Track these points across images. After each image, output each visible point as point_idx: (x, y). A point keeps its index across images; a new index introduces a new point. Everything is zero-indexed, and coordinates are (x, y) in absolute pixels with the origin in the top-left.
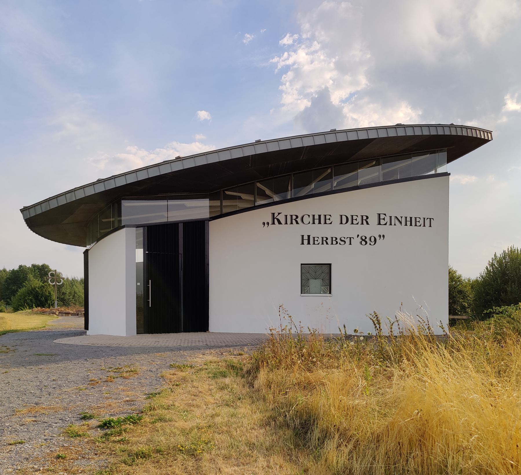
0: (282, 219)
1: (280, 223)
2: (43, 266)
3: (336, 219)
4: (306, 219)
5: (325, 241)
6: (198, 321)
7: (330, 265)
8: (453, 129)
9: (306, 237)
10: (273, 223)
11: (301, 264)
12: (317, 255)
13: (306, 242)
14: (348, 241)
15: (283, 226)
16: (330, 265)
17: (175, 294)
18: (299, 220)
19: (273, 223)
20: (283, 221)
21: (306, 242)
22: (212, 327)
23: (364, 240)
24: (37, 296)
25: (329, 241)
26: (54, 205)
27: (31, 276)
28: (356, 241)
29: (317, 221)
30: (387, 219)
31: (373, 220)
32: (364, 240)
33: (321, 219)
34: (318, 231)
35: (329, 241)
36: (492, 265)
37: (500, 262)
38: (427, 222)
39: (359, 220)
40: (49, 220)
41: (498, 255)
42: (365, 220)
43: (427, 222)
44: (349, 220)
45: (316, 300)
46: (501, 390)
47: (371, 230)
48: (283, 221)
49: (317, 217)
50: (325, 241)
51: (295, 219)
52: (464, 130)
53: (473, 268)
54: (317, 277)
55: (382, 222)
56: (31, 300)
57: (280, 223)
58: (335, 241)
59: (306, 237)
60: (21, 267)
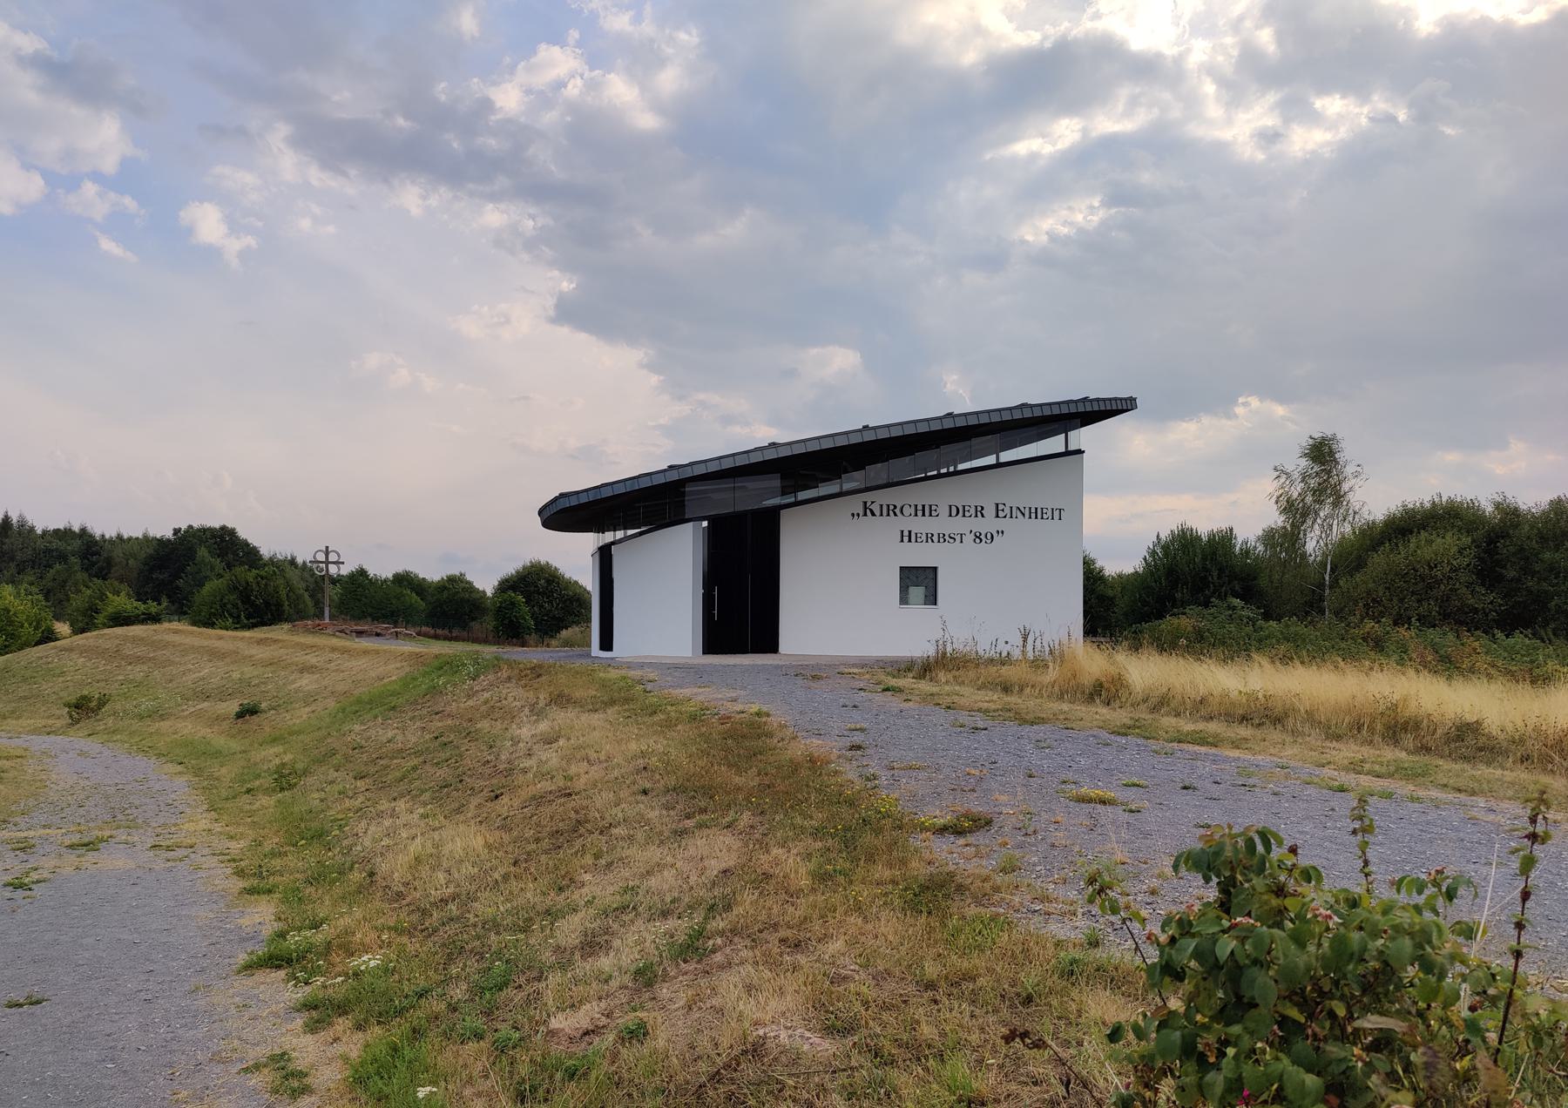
2: (223, 528)
4: (907, 510)
6: (769, 643)
7: (935, 569)
12: (919, 556)
14: (958, 538)
15: (878, 518)
16: (935, 569)
17: (741, 610)
22: (783, 648)
23: (978, 537)
24: (248, 598)
27: (202, 552)
28: (969, 538)
30: (1007, 511)
31: (990, 511)
32: (978, 537)
33: (926, 511)
34: (921, 525)
36: (1153, 553)
37: (1165, 548)
38: (1056, 513)
39: (973, 511)
40: (565, 514)
41: (1163, 536)
42: (980, 511)
43: (1056, 513)
44: (958, 511)
45: (917, 612)
47: (987, 524)
50: (930, 538)
51: (892, 510)
53: (1124, 560)
54: (919, 582)
58: (942, 538)
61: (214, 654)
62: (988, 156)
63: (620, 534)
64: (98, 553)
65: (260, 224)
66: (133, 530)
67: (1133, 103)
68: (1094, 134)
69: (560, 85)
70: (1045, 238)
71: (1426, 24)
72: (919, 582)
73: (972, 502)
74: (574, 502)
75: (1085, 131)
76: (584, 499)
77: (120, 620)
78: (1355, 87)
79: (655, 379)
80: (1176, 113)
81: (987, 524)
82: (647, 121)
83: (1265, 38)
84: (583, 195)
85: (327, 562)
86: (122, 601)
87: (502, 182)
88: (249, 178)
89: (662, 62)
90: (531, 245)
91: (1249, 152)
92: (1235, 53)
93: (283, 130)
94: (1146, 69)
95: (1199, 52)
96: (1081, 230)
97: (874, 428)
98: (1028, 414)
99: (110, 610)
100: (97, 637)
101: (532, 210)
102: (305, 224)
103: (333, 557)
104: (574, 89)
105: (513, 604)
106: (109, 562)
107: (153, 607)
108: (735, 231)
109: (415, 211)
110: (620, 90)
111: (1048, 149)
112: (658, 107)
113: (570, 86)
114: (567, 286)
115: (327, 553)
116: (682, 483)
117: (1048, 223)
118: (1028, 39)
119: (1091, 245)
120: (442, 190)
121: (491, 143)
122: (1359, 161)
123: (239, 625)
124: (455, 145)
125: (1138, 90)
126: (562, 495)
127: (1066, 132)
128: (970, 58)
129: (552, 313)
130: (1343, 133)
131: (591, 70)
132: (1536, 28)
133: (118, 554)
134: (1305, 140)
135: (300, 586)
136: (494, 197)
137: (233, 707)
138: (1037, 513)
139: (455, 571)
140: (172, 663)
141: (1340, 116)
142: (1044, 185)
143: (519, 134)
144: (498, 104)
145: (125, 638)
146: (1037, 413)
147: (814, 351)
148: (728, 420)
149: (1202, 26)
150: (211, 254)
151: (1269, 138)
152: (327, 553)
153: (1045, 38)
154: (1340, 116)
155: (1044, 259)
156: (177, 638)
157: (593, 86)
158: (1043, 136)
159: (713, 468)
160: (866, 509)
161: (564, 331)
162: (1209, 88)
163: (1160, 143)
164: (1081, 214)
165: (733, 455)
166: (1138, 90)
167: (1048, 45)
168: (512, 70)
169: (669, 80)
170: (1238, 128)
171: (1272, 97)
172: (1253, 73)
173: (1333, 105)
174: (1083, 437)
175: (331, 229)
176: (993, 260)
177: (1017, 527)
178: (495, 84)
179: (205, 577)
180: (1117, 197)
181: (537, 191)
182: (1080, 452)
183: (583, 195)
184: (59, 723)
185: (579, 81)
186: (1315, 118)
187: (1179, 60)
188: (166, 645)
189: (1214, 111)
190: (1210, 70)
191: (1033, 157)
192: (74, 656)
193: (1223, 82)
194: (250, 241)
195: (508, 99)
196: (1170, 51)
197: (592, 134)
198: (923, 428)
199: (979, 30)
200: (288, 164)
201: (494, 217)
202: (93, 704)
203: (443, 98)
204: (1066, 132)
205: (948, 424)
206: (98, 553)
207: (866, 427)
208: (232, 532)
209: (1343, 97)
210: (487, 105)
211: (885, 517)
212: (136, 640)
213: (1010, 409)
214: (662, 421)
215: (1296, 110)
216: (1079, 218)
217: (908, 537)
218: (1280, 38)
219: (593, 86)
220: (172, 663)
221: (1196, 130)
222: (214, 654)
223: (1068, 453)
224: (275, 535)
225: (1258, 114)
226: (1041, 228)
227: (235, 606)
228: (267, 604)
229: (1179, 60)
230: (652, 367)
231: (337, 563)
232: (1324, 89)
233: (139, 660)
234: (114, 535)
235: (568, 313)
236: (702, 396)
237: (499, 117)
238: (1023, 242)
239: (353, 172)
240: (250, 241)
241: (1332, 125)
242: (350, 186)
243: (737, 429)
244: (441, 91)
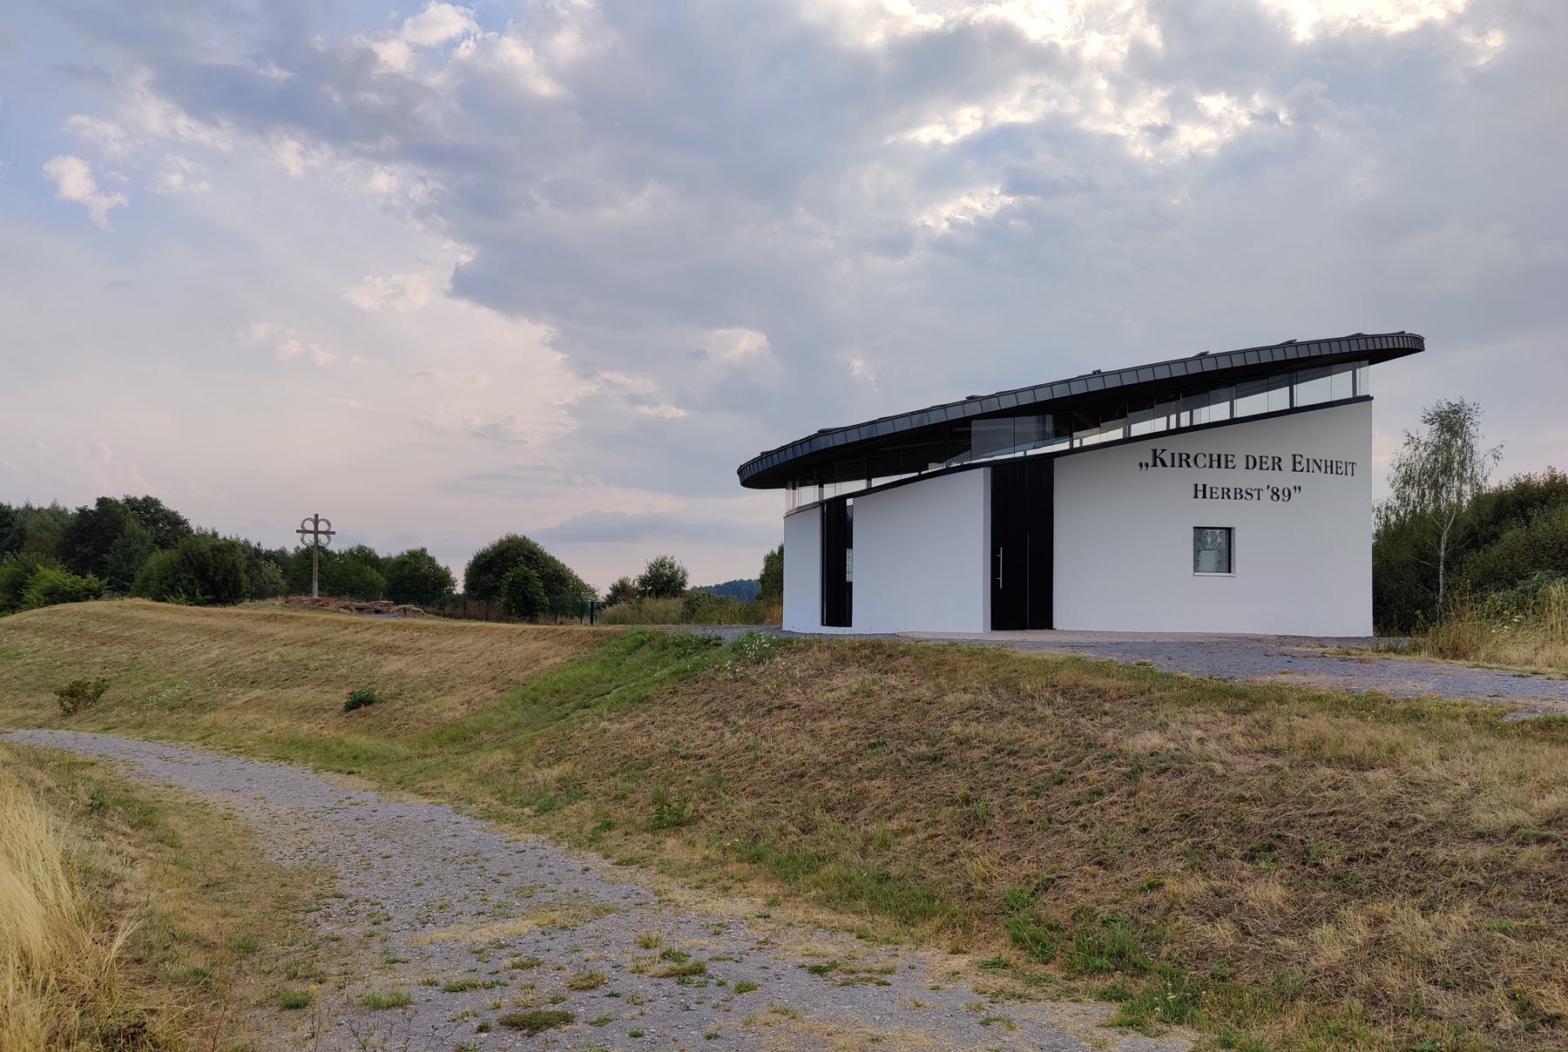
0: (1167, 458)
1: (1164, 465)
2: (146, 499)
3: (1240, 462)
4: (1202, 461)
5: (1226, 493)
8: (1362, 342)
9: (1200, 488)
10: (1155, 465)
11: (1229, 530)
12: (1215, 514)
13: (1200, 494)
14: (1255, 494)
18: (1191, 461)
19: (1155, 465)
20: (1168, 462)
21: (1200, 494)
25: (1232, 494)
26: (883, 430)
28: (1266, 494)
29: (1215, 464)
31: (1287, 464)
33: (1220, 462)
34: (1216, 478)
35: (1232, 494)
39: (1270, 462)
42: (1277, 463)
44: (1255, 463)
45: (1215, 581)
46: (532, 742)
47: (1284, 479)
48: (1168, 462)
49: (1215, 458)
50: (1226, 493)
52: (1362, 342)
54: (1216, 548)
55: (1298, 467)
56: (191, 582)
57: (1164, 465)
58: (1239, 494)
59: (1200, 488)
60: (102, 502)
61: (213, 633)
62: (889, 140)
63: (860, 485)
64: (9, 525)
65: (125, 179)
66: (41, 502)
67: (1032, 92)
68: (994, 124)
69: (452, 44)
70: (945, 225)
71: (1303, 33)
72: (1216, 548)
73: (1270, 452)
74: (839, 440)
75: (985, 120)
76: (853, 437)
77: (56, 596)
78: (1237, 87)
79: (559, 357)
80: (1073, 107)
81: (1284, 479)
82: (545, 88)
83: (1153, 37)
84: (473, 158)
85: (316, 532)
86: (55, 575)
87: (389, 141)
88: (110, 129)
89: (557, 24)
90: (422, 213)
91: (1141, 150)
92: (1125, 49)
93: (142, 76)
94: (1042, 59)
95: (1094, 46)
96: (979, 219)
97: (1215, 356)
98: (1291, 354)
99: (45, 584)
100: (49, 613)
101: (423, 172)
102: (176, 180)
103: (322, 526)
104: (465, 51)
105: (526, 578)
106: (21, 533)
107: (91, 580)
108: (640, 206)
109: (295, 170)
110: (514, 52)
111: (948, 139)
112: (554, 72)
113: (463, 46)
114: (465, 259)
115: (316, 521)
116: (966, 421)
117: (947, 210)
118: (932, 22)
119: (991, 232)
120: (324, 146)
121: (373, 98)
122: (1242, 161)
123: (192, 600)
124: (336, 99)
125: (1036, 81)
126: (822, 433)
127: (968, 120)
128: (875, 38)
129: (448, 286)
130: (1228, 134)
131: (485, 30)
132: (1406, 36)
133: (30, 526)
134: (1194, 137)
135: (242, 564)
136: (383, 158)
137: (341, 697)
138: (1331, 467)
139: (415, 546)
140: (160, 643)
141: (1219, 119)
142: (943, 172)
143: (405, 91)
144: (382, 57)
145: (87, 615)
146: (1303, 353)
147: (720, 332)
148: (635, 400)
149: (1095, 19)
150: (78, 211)
151: (1160, 133)
152: (316, 521)
153: (947, 22)
154: (1219, 119)
155: (944, 246)
156: (143, 614)
157: (485, 48)
158: (948, 125)
159: (1025, 400)
160: (1157, 460)
161: (463, 306)
162: (1102, 85)
163: (1056, 133)
164: (980, 202)
165: (1051, 385)
166: (1036, 81)
167: (951, 28)
168: (398, 25)
169: (566, 44)
170: (1127, 122)
171: (1161, 93)
172: (1143, 68)
173: (1214, 103)
174: (1374, 378)
175: (204, 186)
176: (897, 244)
177: (1313, 482)
178: (377, 39)
179: (124, 548)
180: (1016, 185)
181: (425, 152)
182: (1368, 398)
183: (473, 158)
184: (44, 714)
185: (471, 43)
186: (1200, 117)
187: (1074, 52)
188: (142, 623)
189: (1107, 106)
190: (1100, 66)
191: (936, 144)
192: (27, 635)
193: (1113, 79)
194: (119, 198)
195: (394, 54)
196: (1065, 44)
197: (483, 94)
198: (1146, 377)
199: (882, 12)
200: (156, 116)
201: (383, 181)
202: (90, 692)
203: (320, 48)
204: (968, 120)
205: (1291, 354)
206: (9, 525)
207: (1204, 355)
208: (156, 503)
209: (1229, 95)
210: (368, 57)
211: (1177, 469)
212: (98, 617)
213: (1271, 348)
214: (568, 400)
215: (1182, 107)
216: (979, 206)
217: (1202, 492)
218: (1165, 32)
219: (485, 48)
220: (160, 643)
221: (1088, 124)
222: (213, 633)
223: (1356, 399)
224: (210, 511)
225: (1149, 107)
226: (945, 214)
227: (191, 582)
228: (225, 581)
229: (1074, 52)
230: (555, 345)
231: (327, 533)
232: (1210, 87)
233: (111, 640)
234: (22, 506)
235: (466, 285)
236: (607, 376)
237: (383, 71)
238: (925, 227)
239: (225, 123)
240: (119, 198)
241: (1216, 123)
242: (220, 138)
243: (645, 410)
244: (319, 42)
